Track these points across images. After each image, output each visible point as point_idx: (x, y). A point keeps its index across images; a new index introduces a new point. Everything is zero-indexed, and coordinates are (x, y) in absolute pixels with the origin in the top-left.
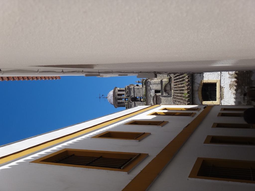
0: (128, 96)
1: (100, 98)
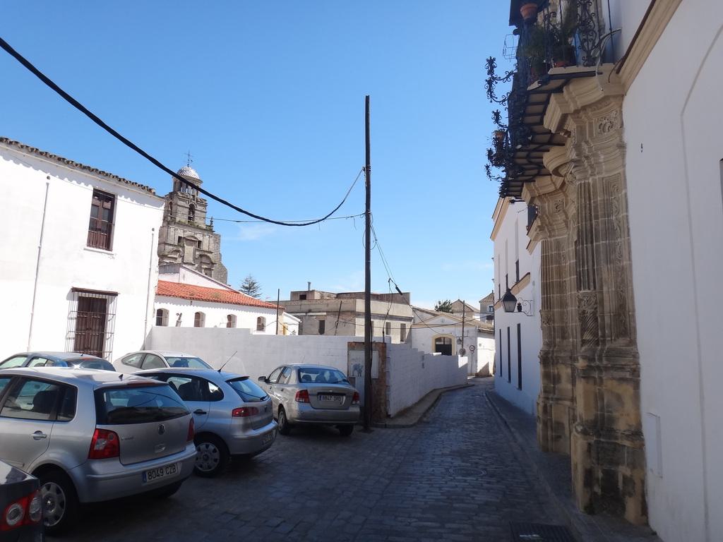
0: (197, 201)
1: (189, 155)
